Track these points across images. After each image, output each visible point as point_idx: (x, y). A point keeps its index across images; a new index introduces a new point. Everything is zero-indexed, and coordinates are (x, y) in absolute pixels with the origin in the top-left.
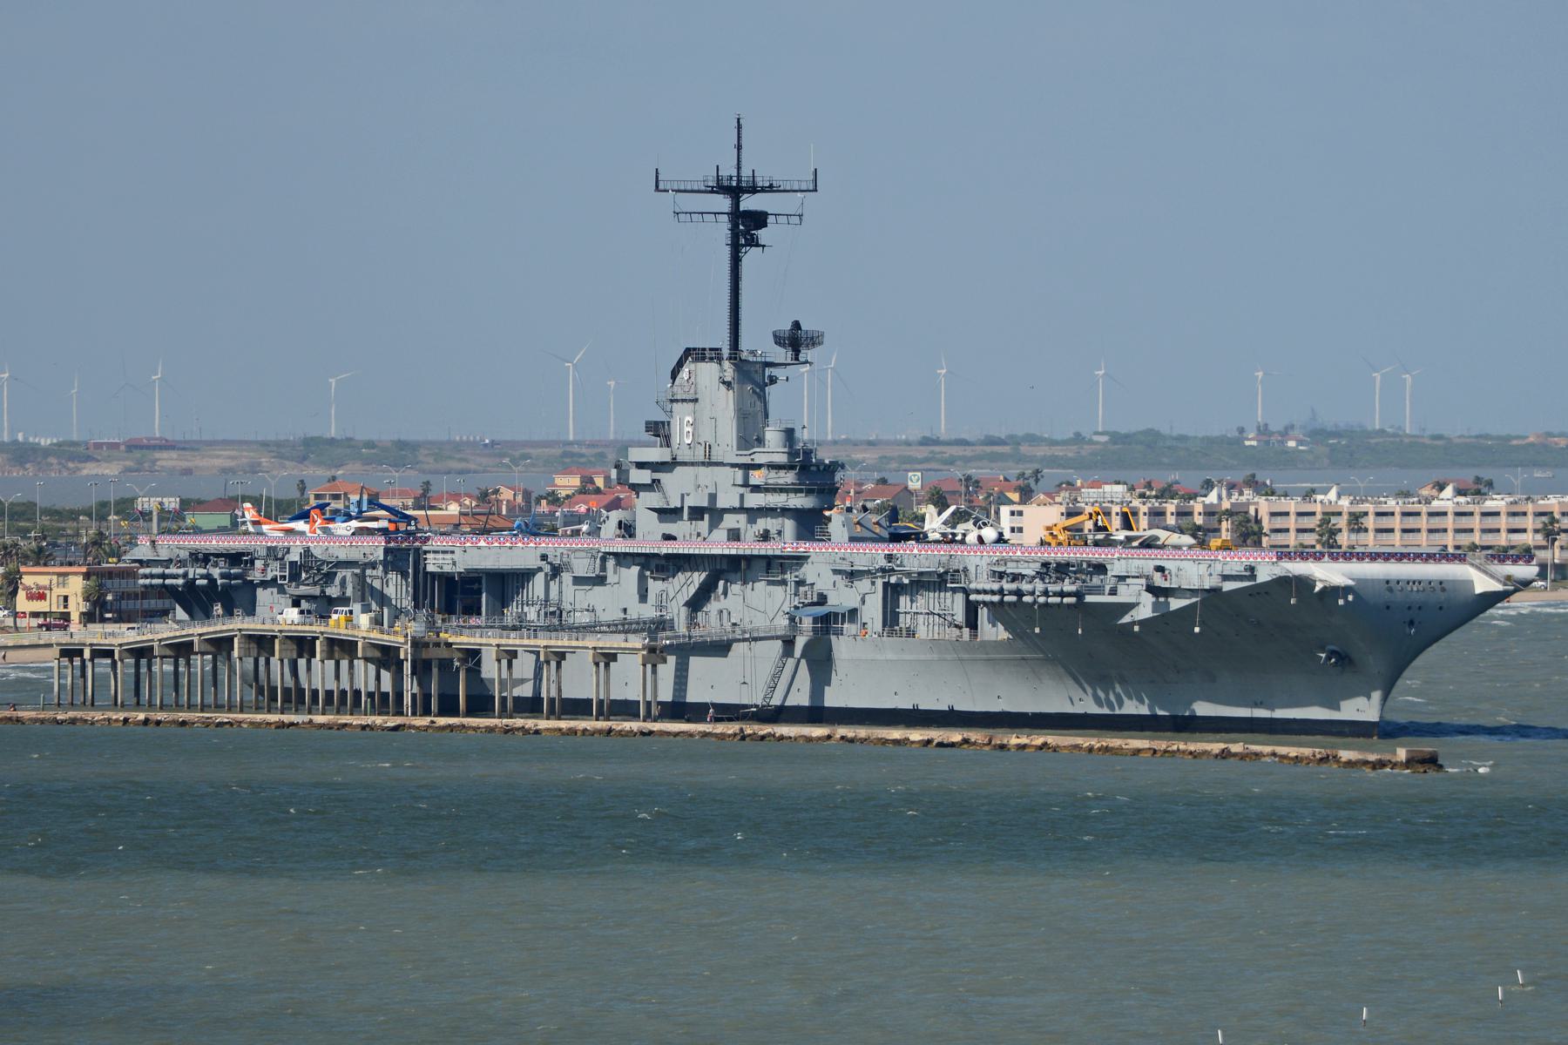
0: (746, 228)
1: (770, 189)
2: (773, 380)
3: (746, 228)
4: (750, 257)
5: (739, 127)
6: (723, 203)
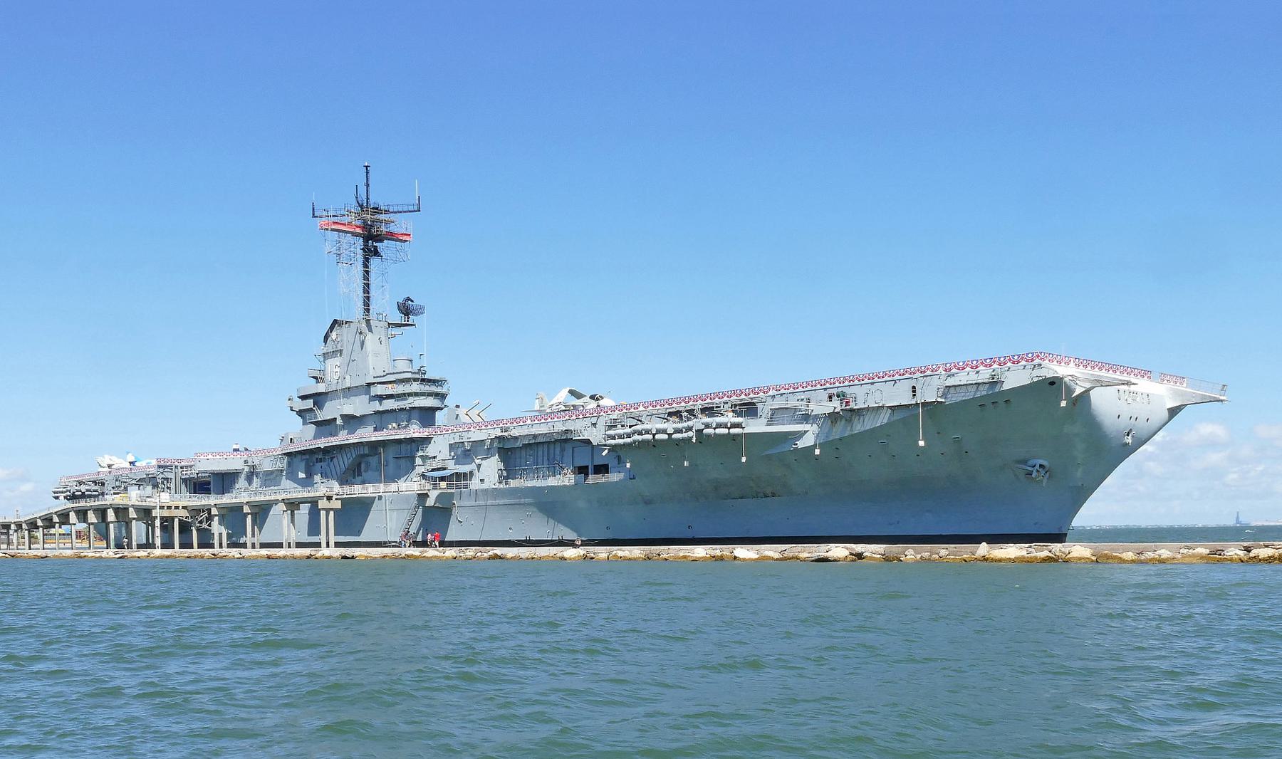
4: (374, 262)
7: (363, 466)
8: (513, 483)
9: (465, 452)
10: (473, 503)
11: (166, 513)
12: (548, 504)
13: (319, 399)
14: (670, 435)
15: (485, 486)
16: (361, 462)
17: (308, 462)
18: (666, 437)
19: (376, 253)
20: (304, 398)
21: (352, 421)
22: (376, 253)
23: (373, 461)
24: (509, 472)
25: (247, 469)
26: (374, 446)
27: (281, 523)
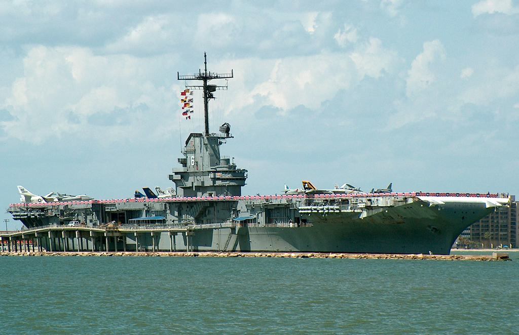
0: (209, 92)
1: (217, 77)
2: (221, 143)
3: (209, 92)
4: (211, 101)
5: (205, 56)
6: (201, 83)
7: (207, 212)
8: (270, 225)
9: (253, 209)
10: (257, 233)
11: (111, 235)
12: (285, 234)
13: (184, 175)
14: (318, 211)
15: (260, 226)
16: (204, 212)
17: (179, 207)
18: (316, 211)
19: (211, 96)
20: (176, 173)
21: (202, 188)
22: (211, 96)
23: (212, 209)
24: (269, 220)
25: (146, 209)
26: (212, 203)
27: (203, 257)
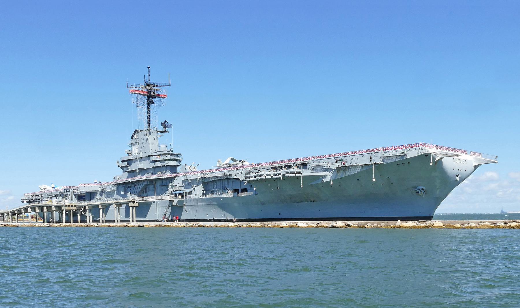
4: (152, 106)
7: (147, 189)
8: (208, 196)
9: (189, 183)
10: (192, 204)
11: (67, 208)
12: (222, 205)
13: (129, 162)
14: (272, 176)
15: (197, 197)
16: (146, 188)
17: (125, 187)
18: (270, 177)
19: (153, 103)
20: (123, 161)
21: (143, 171)
22: (153, 103)
23: (151, 187)
24: (206, 191)
25: (100, 190)
26: (152, 181)
27: (114, 212)
